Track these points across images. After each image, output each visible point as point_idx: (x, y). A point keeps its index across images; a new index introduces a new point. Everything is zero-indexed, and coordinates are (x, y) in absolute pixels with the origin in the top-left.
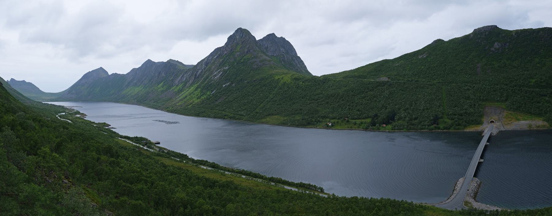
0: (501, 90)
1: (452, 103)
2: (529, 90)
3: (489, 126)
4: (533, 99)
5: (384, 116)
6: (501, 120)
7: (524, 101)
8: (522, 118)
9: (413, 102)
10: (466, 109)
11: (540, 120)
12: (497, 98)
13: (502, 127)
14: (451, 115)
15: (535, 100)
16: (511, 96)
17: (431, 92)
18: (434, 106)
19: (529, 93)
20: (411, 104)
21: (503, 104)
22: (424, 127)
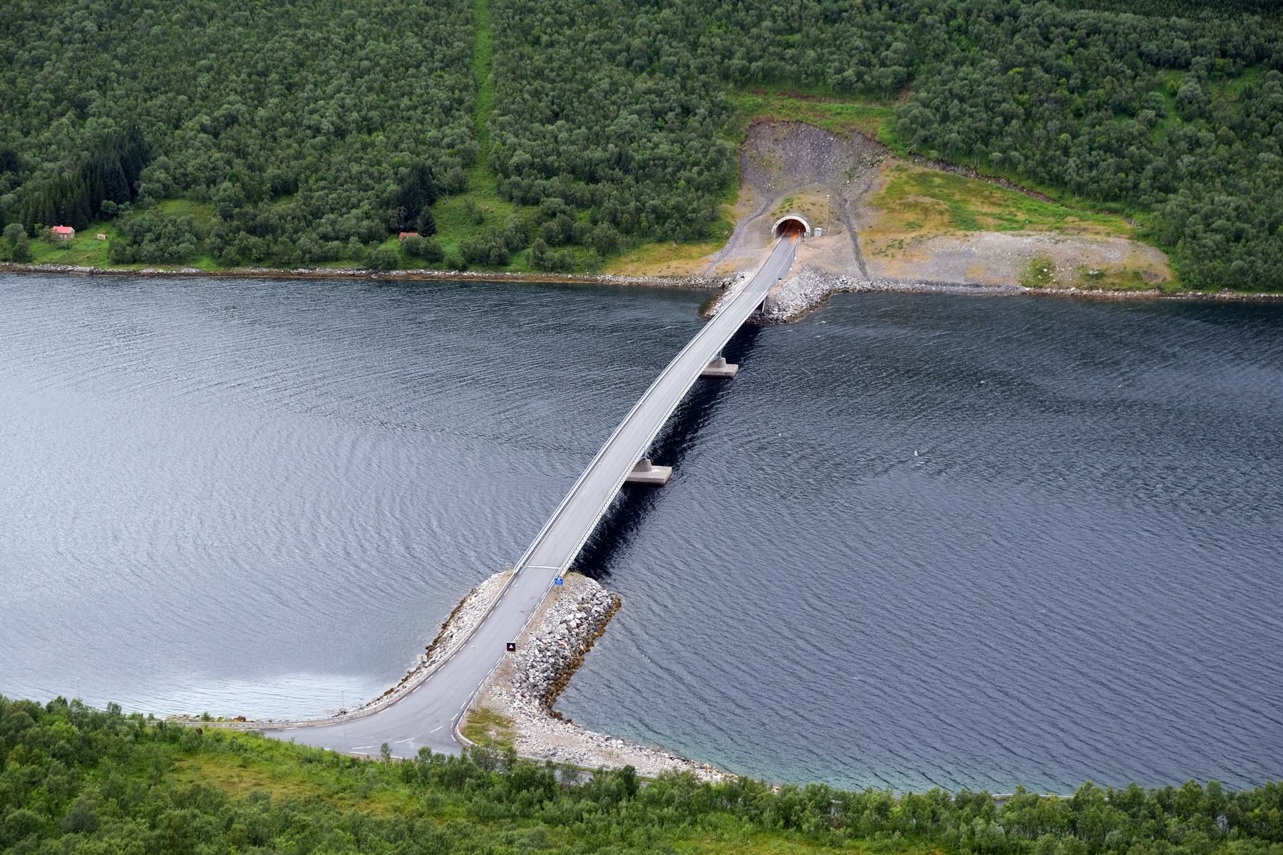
0: (876, 14)
1: (536, 94)
2: (1070, 16)
3: (767, 252)
4: (1084, 87)
5: (62, 170)
6: (854, 222)
7: (1025, 97)
8: (997, 210)
9: (274, 76)
10: (624, 137)
11: (1119, 232)
12: (841, 71)
13: (854, 268)
14: (519, 169)
15: (1101, 91)
16: (938, 56)
17: (398, 13)
18: (415, 108)
19: (1066, 40)
20: (257, 89)
21: (876, 107)
22: (336, 243)
